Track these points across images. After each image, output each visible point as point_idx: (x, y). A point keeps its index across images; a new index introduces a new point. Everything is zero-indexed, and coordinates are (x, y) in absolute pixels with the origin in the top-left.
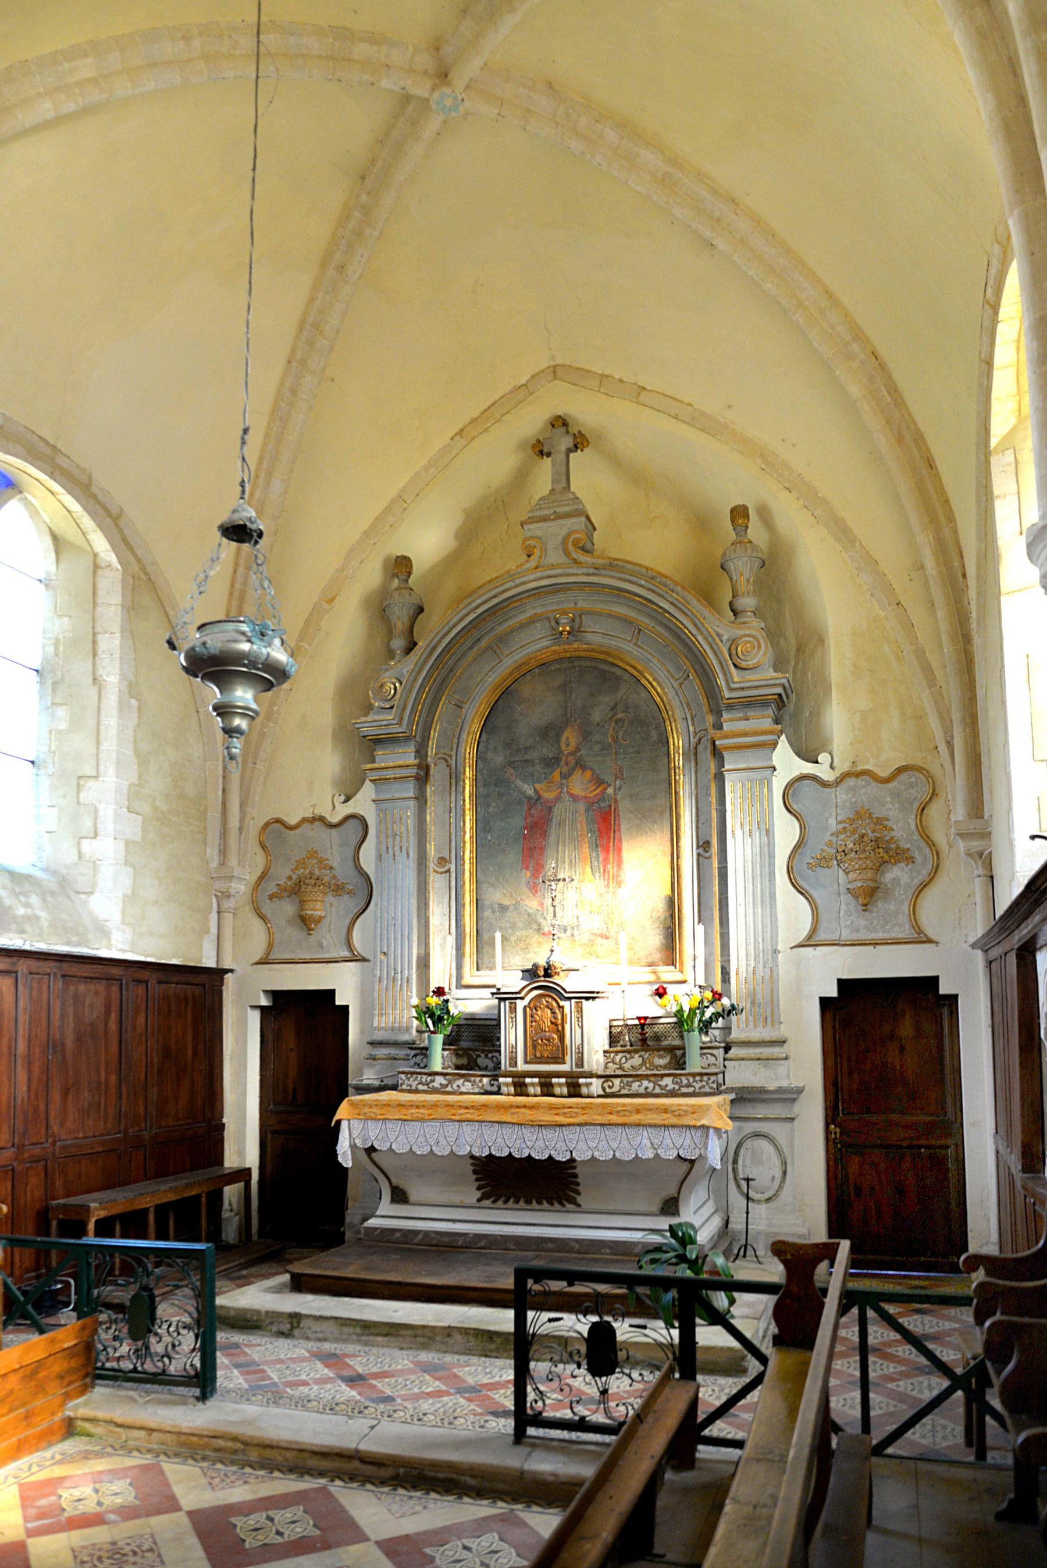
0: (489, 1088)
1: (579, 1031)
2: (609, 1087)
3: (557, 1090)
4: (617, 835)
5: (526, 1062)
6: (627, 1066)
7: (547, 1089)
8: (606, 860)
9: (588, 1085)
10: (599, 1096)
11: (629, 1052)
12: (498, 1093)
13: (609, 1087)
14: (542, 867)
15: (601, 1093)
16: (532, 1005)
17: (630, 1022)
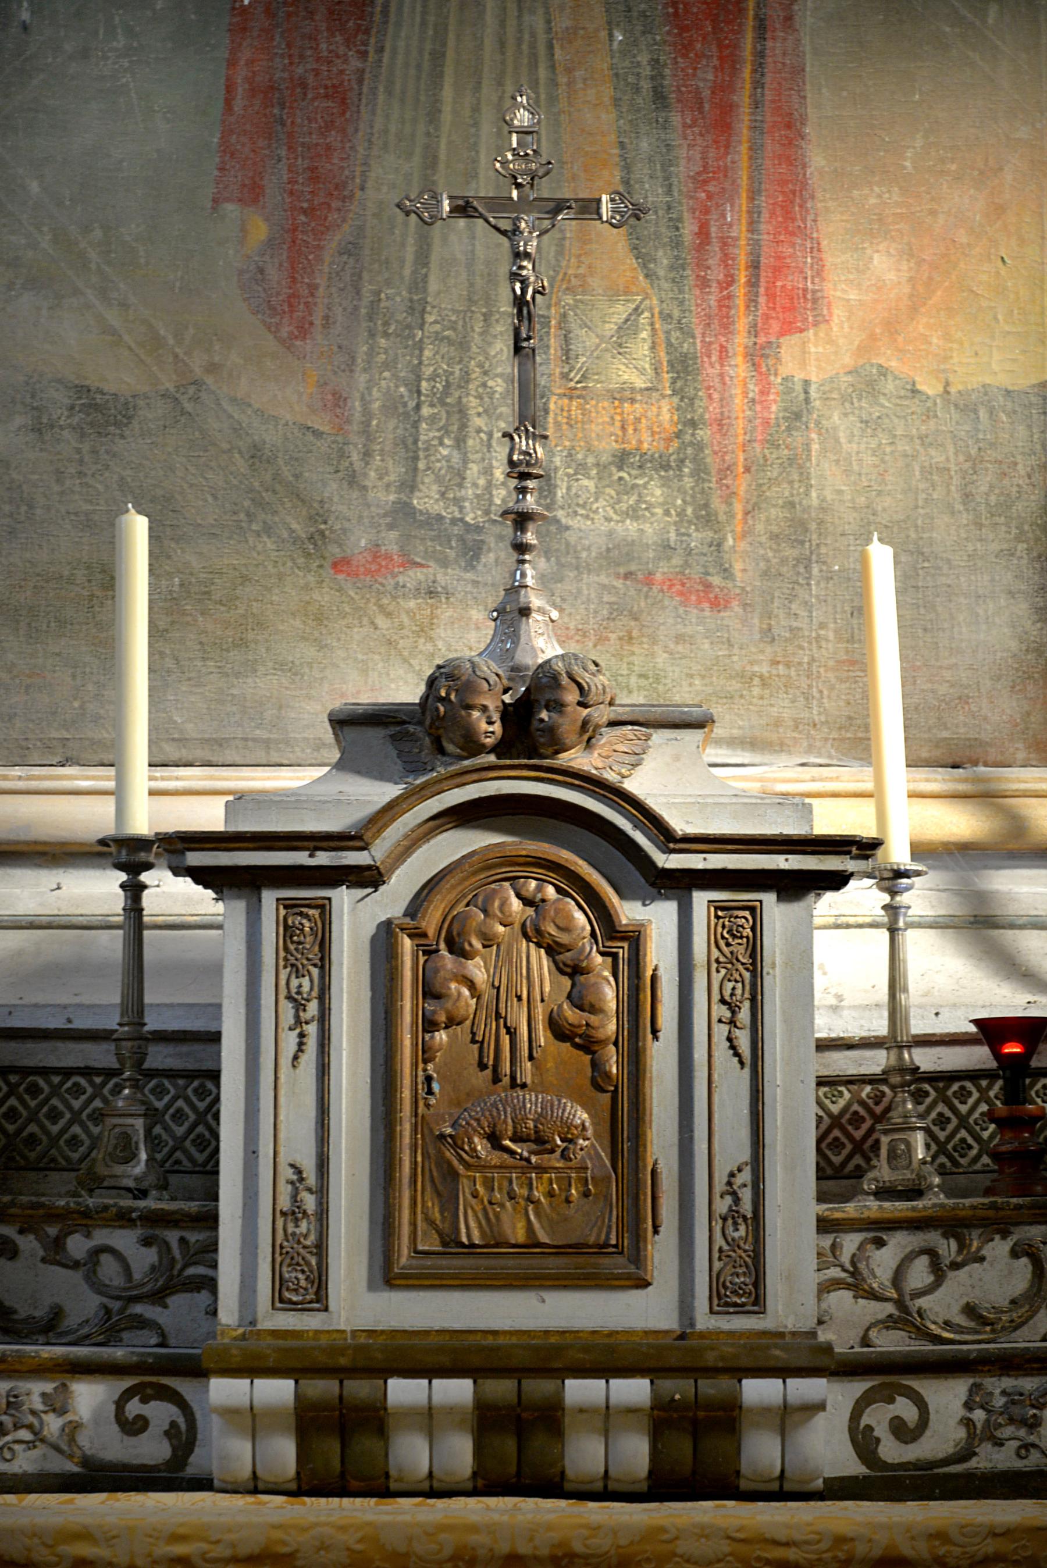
0: (114, 1447)
1: (733, 1081)
2: (901, 1431)
3: (585, 1455)
4: (774, 47)
5: (388, 1276)
6: (942, 1306)
7: (519, 1447)
8: (711, 179)
9: (788, 1418)
10: (839, 1489)
11: (952, 1225)
12: (174, 1475)
13: (901, 1431)
14: (340, 191)
15: (852, 1466)
16: (431, 921)
17: (925, 1059)
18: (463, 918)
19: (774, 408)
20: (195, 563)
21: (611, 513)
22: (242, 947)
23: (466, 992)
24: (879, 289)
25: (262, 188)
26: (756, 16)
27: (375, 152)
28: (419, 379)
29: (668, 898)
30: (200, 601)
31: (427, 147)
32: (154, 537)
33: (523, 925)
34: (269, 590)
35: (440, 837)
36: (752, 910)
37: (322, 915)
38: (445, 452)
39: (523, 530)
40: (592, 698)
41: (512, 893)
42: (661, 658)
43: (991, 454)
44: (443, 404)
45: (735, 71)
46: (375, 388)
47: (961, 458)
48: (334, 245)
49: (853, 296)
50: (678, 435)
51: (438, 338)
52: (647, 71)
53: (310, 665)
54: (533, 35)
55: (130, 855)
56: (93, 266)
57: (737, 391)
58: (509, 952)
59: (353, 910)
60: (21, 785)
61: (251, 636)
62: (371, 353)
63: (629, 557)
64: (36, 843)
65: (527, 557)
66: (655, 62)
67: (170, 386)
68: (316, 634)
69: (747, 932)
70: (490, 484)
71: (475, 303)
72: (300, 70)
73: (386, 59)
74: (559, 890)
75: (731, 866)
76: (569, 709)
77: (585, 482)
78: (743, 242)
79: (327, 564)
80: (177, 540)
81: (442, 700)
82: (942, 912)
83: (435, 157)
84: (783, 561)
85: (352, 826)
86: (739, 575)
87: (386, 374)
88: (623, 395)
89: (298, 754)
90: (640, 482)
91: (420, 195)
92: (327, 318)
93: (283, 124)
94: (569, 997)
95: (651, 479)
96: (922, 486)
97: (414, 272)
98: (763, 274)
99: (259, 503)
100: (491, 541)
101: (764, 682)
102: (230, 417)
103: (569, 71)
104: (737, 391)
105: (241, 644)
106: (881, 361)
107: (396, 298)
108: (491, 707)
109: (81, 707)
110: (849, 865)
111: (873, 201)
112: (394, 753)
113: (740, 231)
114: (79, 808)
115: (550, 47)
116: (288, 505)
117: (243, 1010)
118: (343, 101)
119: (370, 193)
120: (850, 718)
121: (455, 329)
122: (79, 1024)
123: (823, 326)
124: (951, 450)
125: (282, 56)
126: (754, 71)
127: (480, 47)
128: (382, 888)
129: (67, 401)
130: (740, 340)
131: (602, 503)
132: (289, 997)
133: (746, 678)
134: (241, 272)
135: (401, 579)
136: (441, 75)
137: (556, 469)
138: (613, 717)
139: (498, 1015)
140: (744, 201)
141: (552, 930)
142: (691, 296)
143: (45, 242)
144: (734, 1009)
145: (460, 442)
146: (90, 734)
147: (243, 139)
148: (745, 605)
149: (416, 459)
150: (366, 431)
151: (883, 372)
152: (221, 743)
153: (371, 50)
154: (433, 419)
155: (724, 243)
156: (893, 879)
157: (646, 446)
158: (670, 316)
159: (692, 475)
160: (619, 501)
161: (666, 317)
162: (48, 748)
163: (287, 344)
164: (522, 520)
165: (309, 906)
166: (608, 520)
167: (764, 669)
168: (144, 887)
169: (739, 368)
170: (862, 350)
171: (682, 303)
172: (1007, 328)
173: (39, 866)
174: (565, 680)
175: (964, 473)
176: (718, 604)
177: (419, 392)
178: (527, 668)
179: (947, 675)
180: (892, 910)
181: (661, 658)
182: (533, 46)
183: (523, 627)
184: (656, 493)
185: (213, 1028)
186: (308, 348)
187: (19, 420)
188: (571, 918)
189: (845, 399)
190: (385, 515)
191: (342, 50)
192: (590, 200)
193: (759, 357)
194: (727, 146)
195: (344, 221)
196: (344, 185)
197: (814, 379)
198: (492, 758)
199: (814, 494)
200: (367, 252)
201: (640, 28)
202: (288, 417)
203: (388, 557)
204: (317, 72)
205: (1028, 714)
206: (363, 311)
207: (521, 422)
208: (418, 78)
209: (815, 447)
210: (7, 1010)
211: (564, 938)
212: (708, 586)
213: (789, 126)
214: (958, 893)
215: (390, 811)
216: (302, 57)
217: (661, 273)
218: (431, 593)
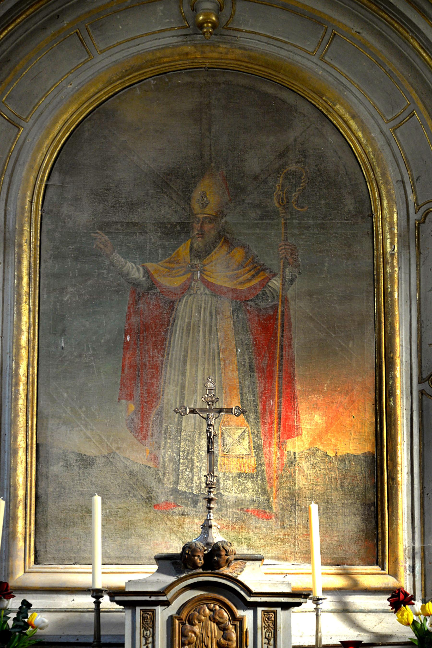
14: (156, 396)
16: (184, 615)
18: (193, 615)
19: (285, 460)
20: (114, 506)
21: (236, 490)
22: (130, 623)
23: (193, 635)
24: (317, 425)
25: (133, 395)
26: (280, 345)
27: (166, 385)
28: (180, 451)
29: (250, 609)
30: (115, 517)
31: (182, 383)
32: (103, 503)
33: (210, 617)
34: (135, 513)
35: (186, 592)
36: (274, 613)
37: (153, 614)
38: (187, 473)
39: (210, 503)
40: (229, 553)
41: (206, 608)
42: (251, 533)
43: (349, 474)
44: (187, 459)
45: (274, 361)
46: (166, 454)
47: (340, 475)
48: (154, 412)
49: (309, 427)
50: (256, 468)
51: (185, 439)
52: (247, 361)
53: (147, 535)
54: (214, 350)
55: (97, 594)
56: (83, 418)
57: (274, 455)
58: (206, 624)
59: (162, 612)
60: (62, 570)
61: (130, 527)
62: (165, 444)
63: (242, 504)
64: (67, 587)
65: (211, 511)
66: (250, 358)
67: (106, 454)
68: (149, 526)
69: (273, 619)
70: (200, 483)
71: (196, 429)
72: (144, 360)
73: (170, 358)
74: (220, 607)
75: (268, 601)
76: (223, 556)
77: (228, 482)
78: (276, 411)
79: (152, 506)
80: (108, 499)
81: (186, 554)
82: (334, 608)
83: (184, 386)
84: (288, 505)
85: (162, 589)
86: (274, 509)
87: (170, 450)
88: (239, 457)
89: (144, 561)
90: (245, 482)
91: (180, 408)
92: (152, 434)
93: (139, 376)
94: (223, 636)
95: (248, 481)
96: (329, 483)
97: (178, 420)
98: (282, 421)
99: (132, 488)
100: (201, 499)
101: (282, 541)
102: (124, 463)
103: (224, 361)
104: (274, 455)
105: (127, 529)
106: (317, 446)
107: (173, 428)
108: (201, 556)
109: (80, 548)
110: (302, 600)
111: (315, 399)
112: (173, 568)
113: (275, 408)
114: (78, 576)
115: (219, 353)
116: (141, 489)
117: (131, 640)
118: (157, 370)
119: (165, 397)
120: (307, 551)
121: (190, 437)
122: (80, 641)
123: (300, 436)
124: (337, 472)
125: (139, 356)
126: (279, 361)
127: (198, 354)
128: (170, 606)
129: (75, 458)
130: (275, 440)
131: (234, 488)
132: (144, 636)
133: (276, 539)
134: (127, 420)
135: (174, 510)
136: (186, 362)
137: (220, 478)
138: (235, 557)
139: (202, 642)
140: (276, 399)
141: (218, 618)
142: (260, 427)
143: (69, 411)
144: (269, 640)
145: (192, 470)
146: (82, 556)
147: (127, 381)
148: (276, 518)
149: (179, 475)
150: (164, 467)
151: (317, 449)
152: (121, 558)
153: (165, 354)
154: (184, 463)
155: (270, 411)
156: (317, 601)
157: (247, 471)
158: (254, 433)
159: (260, 480)
160: (239, 488)
161: (253, 433)
162: (70, 559)
163: (140, 441)
164: (210, 500)
165: (149, 611)
166: (236, 493)
167: (282, 537)
168: (100, 603)
169: (274, 448)
170: (311, 443)
171: (258, 429)
172: (354, 437)
173: (68, 594)
174: (222, 549)
175: (341, 480)
176: (268, 517)
177: (180, 455)
178: (211, 543)
179: (336, 538)
180: (317, 609)
181: (251, 533)
182: (214, 353)
183: (210, 531)
184: (250, 485)
185: (120, 641)
186: (147, 443)
187: (61, 464)
188: (223, 615)
189: (306, 457)
190: (169, 492)
191: (157, 354)
192: (230, 409)
193: (281, 445)
194: (271, 383)
195: (157, 405)
196: (157, 394)
197: (297, 451)
198: (201, 570)
199: (297, 485)
200: (164, 414)
201: (245, 348)
202: (141, 463)
203: (170, 504)
204: (149, 361)
205: (360, 550)
206: (163, 432)
207: (209, 472)
208: (179, 363)
209: (297, 472)
210: (59, 637)
211: (221, 620)
212: (265, 512)
213: (290, 377)
214: (338, 602)
215: (173, 585)
216: (145, 356)
217: (252, 420)
218: (183, 514)
